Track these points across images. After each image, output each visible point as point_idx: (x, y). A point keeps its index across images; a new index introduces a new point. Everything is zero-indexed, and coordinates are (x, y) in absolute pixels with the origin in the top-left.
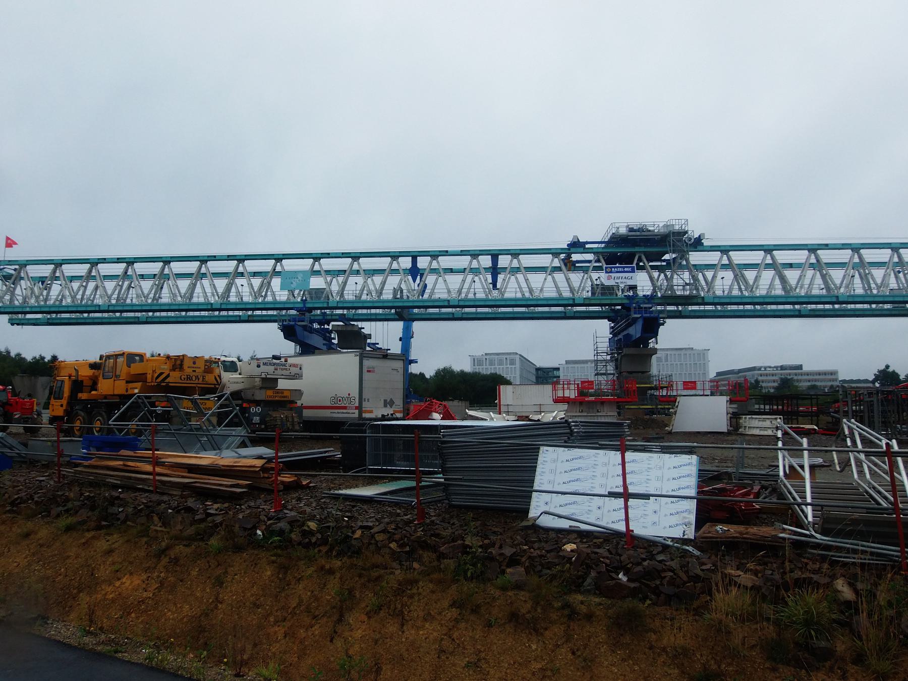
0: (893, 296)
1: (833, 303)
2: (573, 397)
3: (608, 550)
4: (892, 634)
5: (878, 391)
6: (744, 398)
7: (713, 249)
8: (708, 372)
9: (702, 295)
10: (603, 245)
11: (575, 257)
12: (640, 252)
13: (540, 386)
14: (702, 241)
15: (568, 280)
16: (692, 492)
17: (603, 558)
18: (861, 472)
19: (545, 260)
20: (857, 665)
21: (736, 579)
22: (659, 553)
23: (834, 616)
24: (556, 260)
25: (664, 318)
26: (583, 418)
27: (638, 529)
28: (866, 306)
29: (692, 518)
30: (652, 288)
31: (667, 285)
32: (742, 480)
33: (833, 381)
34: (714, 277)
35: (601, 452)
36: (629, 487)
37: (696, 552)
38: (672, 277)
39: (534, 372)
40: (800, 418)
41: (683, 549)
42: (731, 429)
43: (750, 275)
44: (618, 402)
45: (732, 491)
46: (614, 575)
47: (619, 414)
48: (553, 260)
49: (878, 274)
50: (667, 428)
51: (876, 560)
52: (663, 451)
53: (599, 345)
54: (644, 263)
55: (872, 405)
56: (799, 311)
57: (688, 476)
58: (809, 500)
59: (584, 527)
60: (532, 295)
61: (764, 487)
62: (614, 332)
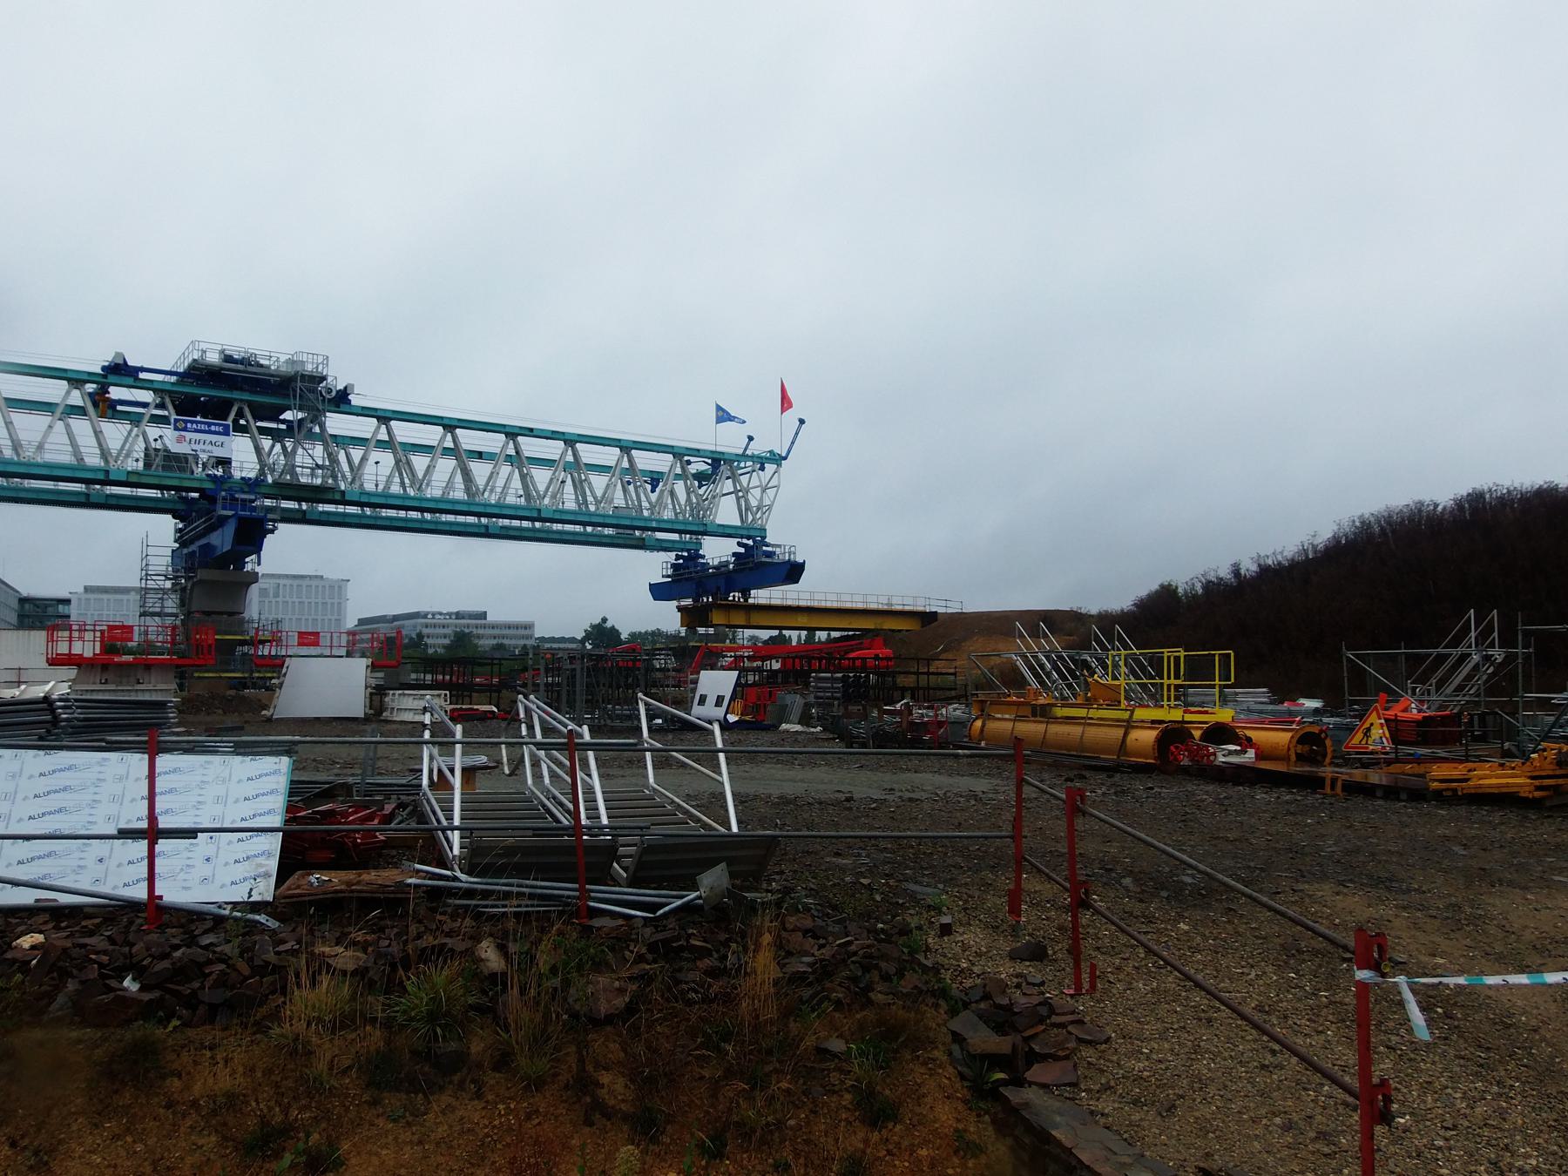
0: (617, 517)
1: (533, 520)
2: (88, 654)
3: (108, 937)
4: (554, 1016)
5: (584, 655)
6: (394, 662)
7: (366, 412)
8: (345, 618)
9: (343, 488)
10: (173, 379)
11: (116, 393)
12: (241, 400)
13: (21, 632)
14: (350, 397)
15: (98, 434)
16: (277, 821)
17: (97, 953)
18: (538, 776)
19: (54, 391)
20: (500, 1072)
21: (330, 961)
22: (206, 932)
23: (471, 1000)
24: (76, 394)
25: (274, 521)
26: (107, 694)
27: (172, 892)
28: (578, 528)
29: (273, 865)
30: (258, 467)
31: (285, 465)
32: (370, 796)
33: (527, 638)
34: (364, 459)
35: (113, 756)
36: (160, 819)
37: (273, 924)
38: (294, 451)
39: (15, 605)
40: (474, 694)
41: (248, 920)
42: (372, 712)
43: (420, 462)
44: (178, 666)
45: (345, 815)
46: (113, 983)
47: (181, 687)
48: (68, 393)
49: (599, 482)
50: (264, 712)
51: (538, 906)
52: (238, 751)
53: (152, 560)
54: (247, 421)
55: (574, 677)
56: (486, 527)
57: (272, 792)
58: (457, 822)
59: (65, 899)
60: (18, 454)
61: (402, 806)
62: (182, 539)
